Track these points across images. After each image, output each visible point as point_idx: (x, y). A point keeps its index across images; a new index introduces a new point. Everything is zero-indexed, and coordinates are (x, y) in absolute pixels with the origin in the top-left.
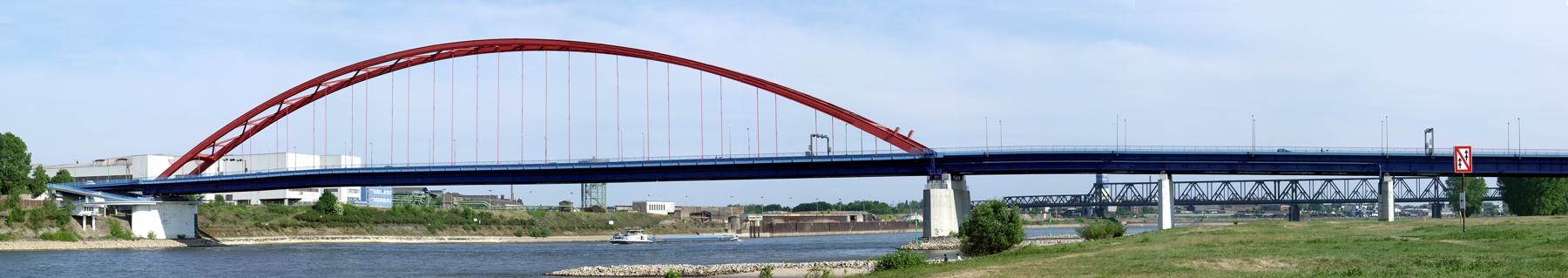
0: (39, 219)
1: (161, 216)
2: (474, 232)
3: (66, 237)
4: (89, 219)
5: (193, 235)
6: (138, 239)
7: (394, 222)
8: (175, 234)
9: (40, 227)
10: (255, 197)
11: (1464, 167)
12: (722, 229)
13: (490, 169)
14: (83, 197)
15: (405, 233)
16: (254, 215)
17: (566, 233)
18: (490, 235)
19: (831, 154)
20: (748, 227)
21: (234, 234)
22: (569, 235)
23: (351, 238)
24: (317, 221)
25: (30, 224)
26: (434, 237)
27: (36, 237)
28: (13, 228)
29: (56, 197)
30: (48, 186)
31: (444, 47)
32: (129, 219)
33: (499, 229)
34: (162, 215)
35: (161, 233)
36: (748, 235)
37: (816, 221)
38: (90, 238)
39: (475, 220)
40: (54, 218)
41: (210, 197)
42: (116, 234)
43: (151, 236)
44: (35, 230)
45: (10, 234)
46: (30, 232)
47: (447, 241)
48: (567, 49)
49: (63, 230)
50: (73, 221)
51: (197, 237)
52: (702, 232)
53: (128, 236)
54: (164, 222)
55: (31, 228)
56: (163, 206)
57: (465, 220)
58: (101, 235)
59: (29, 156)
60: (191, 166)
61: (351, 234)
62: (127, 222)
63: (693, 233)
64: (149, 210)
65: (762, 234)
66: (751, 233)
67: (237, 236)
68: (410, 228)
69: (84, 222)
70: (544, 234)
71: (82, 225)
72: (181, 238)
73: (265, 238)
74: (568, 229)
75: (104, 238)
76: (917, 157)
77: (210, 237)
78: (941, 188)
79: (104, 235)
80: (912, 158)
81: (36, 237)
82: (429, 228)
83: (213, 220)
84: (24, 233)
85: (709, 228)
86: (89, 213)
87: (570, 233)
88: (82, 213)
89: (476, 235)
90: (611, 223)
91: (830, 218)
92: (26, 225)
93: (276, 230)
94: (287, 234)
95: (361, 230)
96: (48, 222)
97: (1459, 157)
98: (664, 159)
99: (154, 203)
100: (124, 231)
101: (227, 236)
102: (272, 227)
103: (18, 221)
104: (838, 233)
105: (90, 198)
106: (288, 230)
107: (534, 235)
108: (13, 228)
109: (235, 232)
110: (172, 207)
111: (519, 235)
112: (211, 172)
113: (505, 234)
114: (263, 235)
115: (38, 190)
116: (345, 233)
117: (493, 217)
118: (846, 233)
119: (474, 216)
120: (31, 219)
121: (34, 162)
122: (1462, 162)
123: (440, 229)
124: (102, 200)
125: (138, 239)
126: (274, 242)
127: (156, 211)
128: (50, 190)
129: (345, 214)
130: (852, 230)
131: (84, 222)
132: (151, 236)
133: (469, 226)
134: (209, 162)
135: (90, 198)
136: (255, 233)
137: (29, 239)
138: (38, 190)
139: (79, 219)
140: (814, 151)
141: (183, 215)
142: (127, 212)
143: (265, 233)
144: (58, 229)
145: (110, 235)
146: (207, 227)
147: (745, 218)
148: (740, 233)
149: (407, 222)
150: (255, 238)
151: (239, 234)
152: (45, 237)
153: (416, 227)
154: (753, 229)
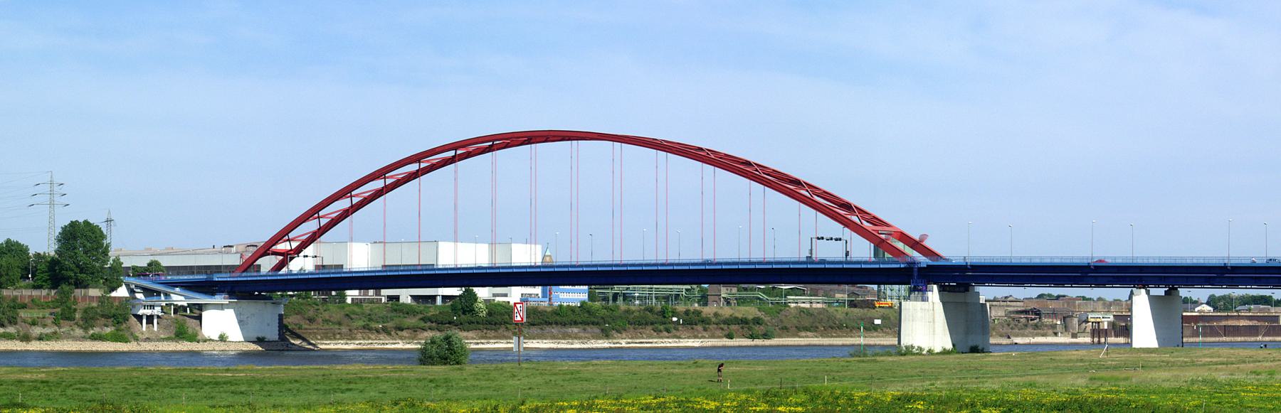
0: (92, 318)
1: (237, 316)
2: (667, 334)
3: (117, 338)
4: (150, 319)
5: (276, 337)
6: (205, 341)
7: (556, 323)
8: (254, 336)
9: (92, 326)
10: (405, 295)
11: (519, 319)
12: (1051, 332)
13: (859, 266)
14: (159, 293)
15: (566, 336)
16: (369, 315)
17: (803, 334)
18: (689, 338)
19: (848, 259)
20: (1088, 330)
21: (332, 336)
22: (807, 337)
23: (488, 343)
24: (450, 323)
25: (81, 323)
26: (607, 341)
27: (84, 337)
28: (60, 327)
29: (135, 292)
30: (127, 279)
31: (498, 137)
32: (199, 318)
33: (705, 330)
34: (238, 315)
35: (235, 335)
36: (1088, 340)
37: (1223, 323)
38: (148, 339)
39: (675, 319)
40: (110, 317)
41: (352, 294)
42: (181, 335)
43: (222, 338)
44: (86, 329)
45: (55, 333)
46: (79, 332)
47: (624, 345)
48: (570, 139)
49: (117, 330)
50: (134, 319)
51: (282, 338)
52: (1017, 336)
53: (193, 338)
54: (241, 322)
55: (82, 328)
56: (239, 305)
57: (660, 318)
58: (162, 336)
59: (108, 246)
60: (267, 264)
61: (490, 338)
62: (198, 322)
63: (1001, 336)
64: (222, 309)
65: (1112, 340)
66: (1093, 337)
67: (335, 339)
68: (575, 330)
69: (144, 321)
70: (766, 336)
71: (142, 324)
72: (260, 341)
73: (370, 341)
74: (806, 329)
75: (168, 339)
76: (902, 266)
77: (304, 339)
78: (923, 301)
79: (166, 337)
80: (898, 266)
81: (84, 337)
82: (602, 330)
83: (311, 320)
84: (72, 333)
85: (1029, 330)
86: (148, 312)
87: (809, 333)
88: (141, 312)
89: (668, 338)
90: (878, 322)
91: (1250, 318)
92: (76, 324)
93: (389, 334)
94: (401, 338)
95: (506, 334)
96: (103, 320)
97: (516, 310)
98: (792, 260)
99: (226, 302)
100: (190, 331)
101: (322, 339)
102: (386, 331)
103: (68, 319)
104: (1239, 339)
105: (167, 295)
106: (405, 333)
107: (752, 337)
108: (60, 327)
109: (334, 335)
110: (250, 307)
111: (730, 337)
112: (296, 265)
113: (713, 337)
114: (369, 338)
115: (115, 285)
116: (482, 338)
117: (703, 315)
118: (1253, 339)
119: (674, 314)
120: (82, 319)
121: (112, 254)
122: (518, 314)
123: (618, 331)
124: (182, 298)
125: (205, 341)
126: (382, 346)
127: (231, 311)
128: (128, 286)
129: (490, 314)
130: (1264, 336)
131: (144, 321)
132: (222, 338)
133: (662, 327)
134: (287, 256)
135: (167, 295)
136: (359, 335)
137: (75, 339)
138: (115, 285)
139: (139, 318)
140: (814, 256)
141: (266, 317)
142: (196, 312)
143: (373, 337)
144: (113, 328)
145: (173, 336)
146: (299, 328)
147: (1084, 318)
148: (1076, 338)
149: (576, 323)
150: (357, 342)
151: (338, 336)
152: (94, 338)
153: (585, 329)
154: (1097, 332)
